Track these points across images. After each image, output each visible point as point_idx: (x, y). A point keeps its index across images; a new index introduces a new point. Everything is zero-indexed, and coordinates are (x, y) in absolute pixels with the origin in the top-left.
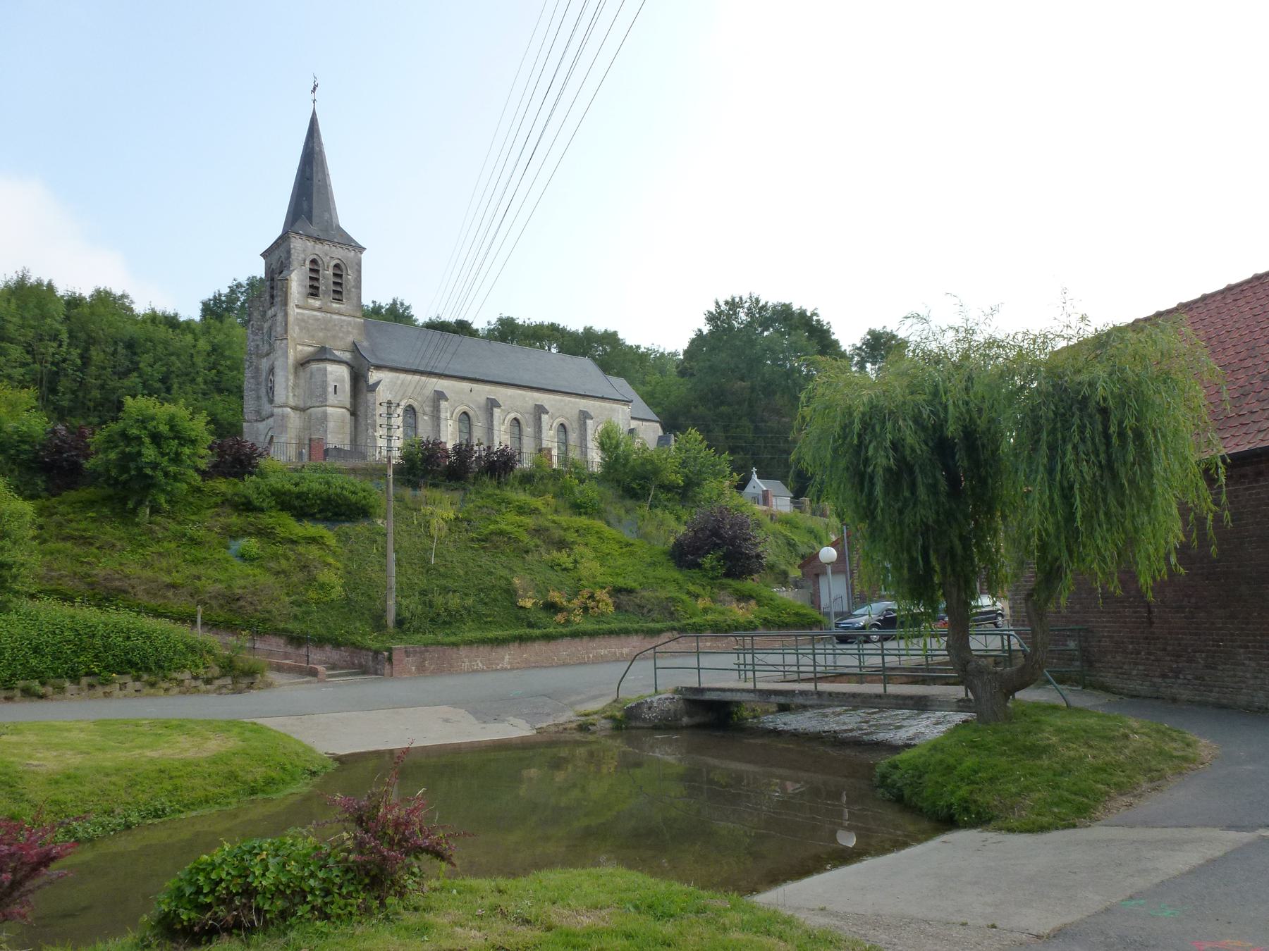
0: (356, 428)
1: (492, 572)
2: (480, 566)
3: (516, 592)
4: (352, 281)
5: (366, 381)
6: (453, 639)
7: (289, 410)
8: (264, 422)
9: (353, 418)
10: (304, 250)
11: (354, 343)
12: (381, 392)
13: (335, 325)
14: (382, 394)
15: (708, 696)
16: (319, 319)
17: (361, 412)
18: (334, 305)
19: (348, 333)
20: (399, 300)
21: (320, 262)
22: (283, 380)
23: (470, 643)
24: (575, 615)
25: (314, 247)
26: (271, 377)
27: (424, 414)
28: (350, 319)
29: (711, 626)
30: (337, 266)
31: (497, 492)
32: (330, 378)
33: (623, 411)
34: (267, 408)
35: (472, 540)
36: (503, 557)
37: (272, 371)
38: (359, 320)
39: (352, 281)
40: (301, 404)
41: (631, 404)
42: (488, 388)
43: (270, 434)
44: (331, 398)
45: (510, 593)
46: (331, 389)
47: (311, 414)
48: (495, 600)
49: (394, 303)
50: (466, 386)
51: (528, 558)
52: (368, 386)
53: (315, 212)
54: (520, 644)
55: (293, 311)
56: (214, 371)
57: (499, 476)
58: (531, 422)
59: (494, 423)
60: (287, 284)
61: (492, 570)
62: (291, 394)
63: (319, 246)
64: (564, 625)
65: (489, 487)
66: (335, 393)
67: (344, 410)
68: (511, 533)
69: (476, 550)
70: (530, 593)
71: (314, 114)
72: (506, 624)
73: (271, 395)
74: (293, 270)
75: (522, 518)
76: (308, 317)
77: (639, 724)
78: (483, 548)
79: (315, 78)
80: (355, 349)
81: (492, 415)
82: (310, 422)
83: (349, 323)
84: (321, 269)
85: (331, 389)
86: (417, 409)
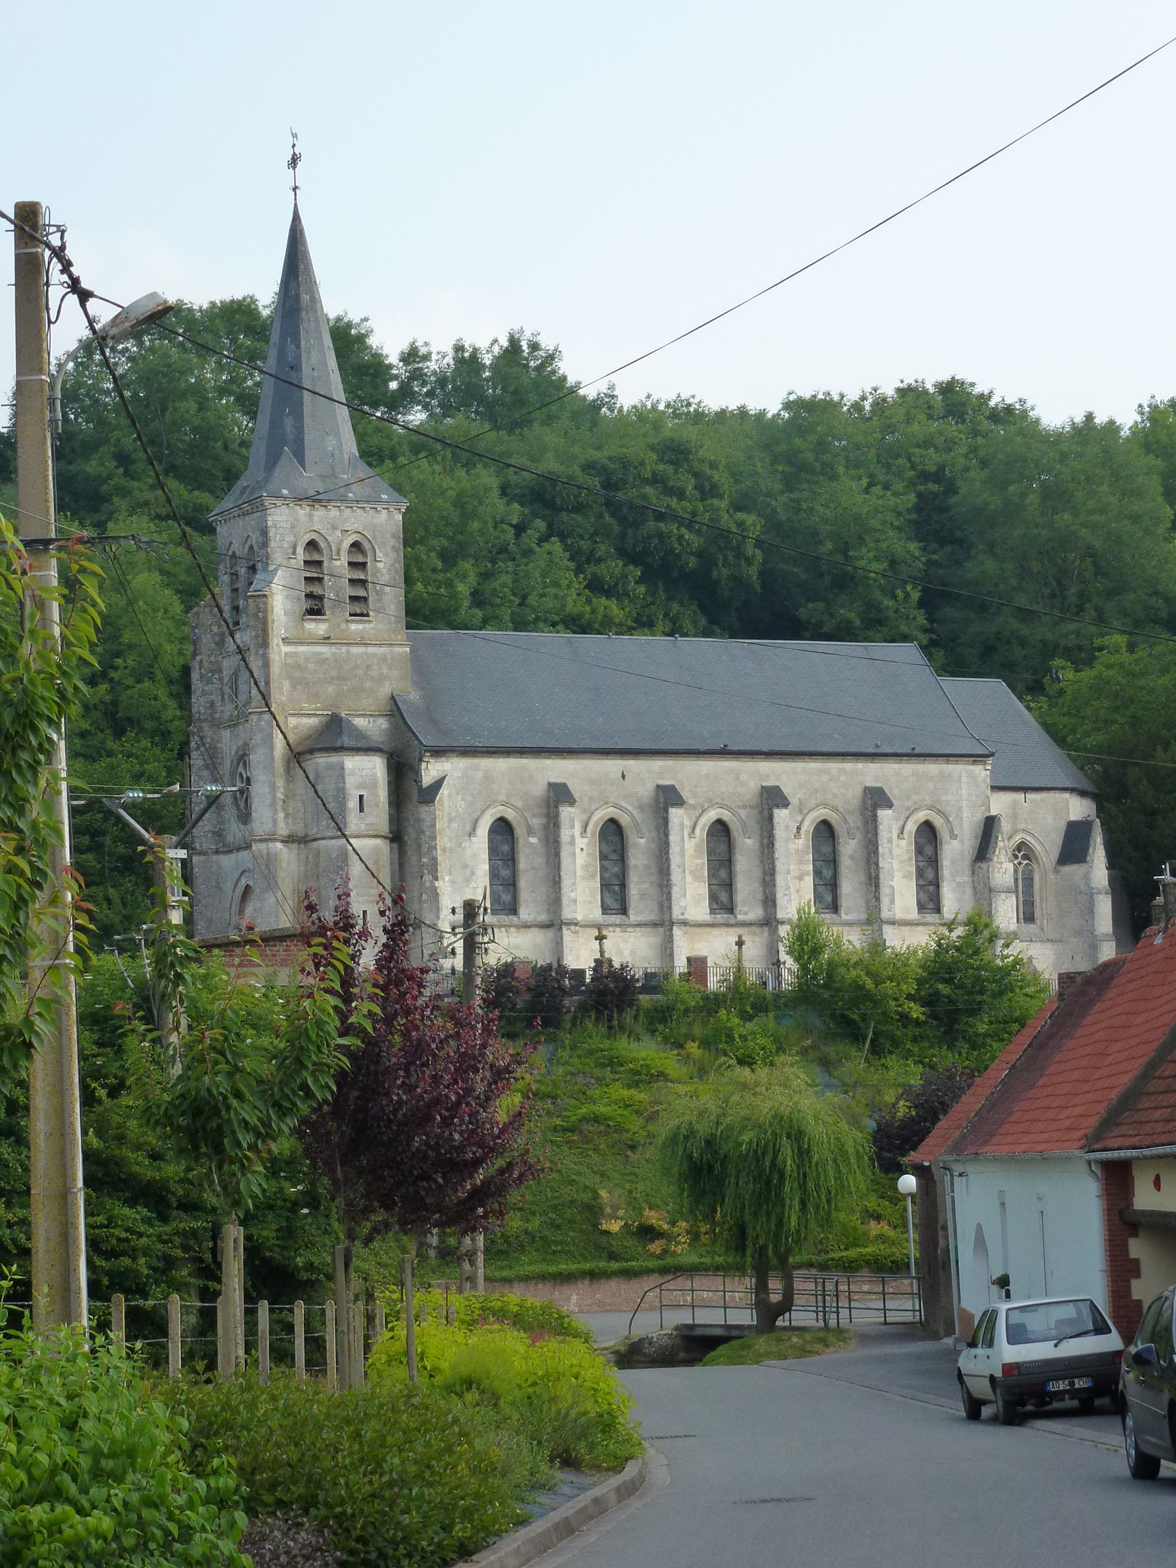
0: (401, 865)
1: (574, 1181)
2: (559, 1171)
3: (601, 1209)
4: (384, 571)
5: (418, 781)
6: (506, 1273)
7: (279, 845)
8: (232, 856)
9: (395, 845)
10: (293, 527)
11: (393, 697)
12: (445, 798)
13: (357, 667)
14: (448, 803)
15: (699, 1332)
16: (325, 660)
17: (410, 836)
18: (353, 627)
19: (381, 678)
20: (528, 334)
21: (323, 545)
22: (267, 790)
23: (526, 1279)
24: (678, 1243)
25: (311, 516)
26: (241, 769)
27: (530, 831)
28: (382, 650)
29: (868, 1262)
30: (356, 545)
31: (607, 1044)
32: (351, 782)
33: (971, 776)
34: (234, 831)
35: (555, 1129)
36: (595, 1156)
37: (242, 758)
38: (400, 650)
39: (384, 571)
40: (300, 830)
41: (990, 761)
42: (657, 764)
43: (243, 882)
44: (354, 822)
45: (593, 1211)
46: (353, 804)
47: (318, 853)
48: (571, 1221)
49: (514, 343)
50: (612, 766)
51: (633, 1156)
52: (421, 790)
53: (309, 438)
54: (591, 1281)
55: (279, 651)
56: (104, 687)
57: (610, 1020)
58: (753, 824)
59: (671, 838)
60: (265, 604)
61: (574, 1177)
62: (282, 815)
63: (319, 513)
64: (658, 1257)
65: (595, 1037)
66: (361, 810)
67: (378, 841)
68: (610, 1119)
69: (559, 1146)
70: (621, 1213)
71: (296, 218)
72: (581, 1255)
73: (242, 804)
74: (276, 570)
75: (633, 1091)
76: (307, 659)
77: (642, 1359)
78: (568, 1142)
79: (295, 136)
80: (394, 710)
81: (666, 821)
82: (317, 866)
83: (383, 659)
84: (325, 559)
85: (353, 804)
86: (514, 824)
